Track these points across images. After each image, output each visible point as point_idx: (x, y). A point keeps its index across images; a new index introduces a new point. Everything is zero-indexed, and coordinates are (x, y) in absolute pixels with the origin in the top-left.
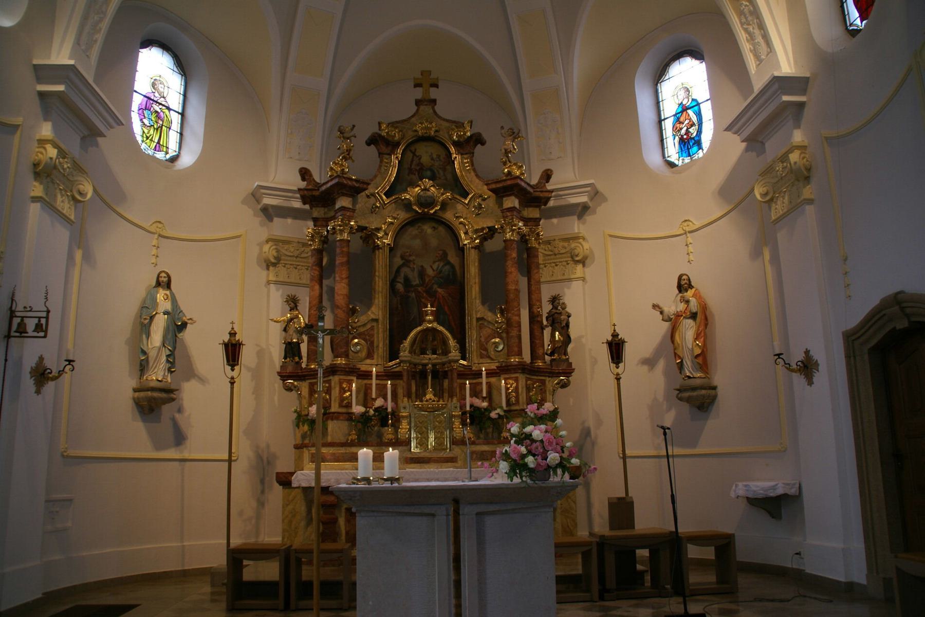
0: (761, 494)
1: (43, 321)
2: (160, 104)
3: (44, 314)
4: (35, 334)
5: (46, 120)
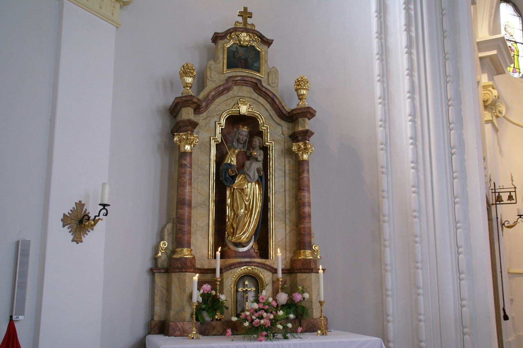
0: (179, 157)
1: (513, 194)
2: (511, 41)
3: (513, 190)
4: (509, 202)
5: (483, 73)
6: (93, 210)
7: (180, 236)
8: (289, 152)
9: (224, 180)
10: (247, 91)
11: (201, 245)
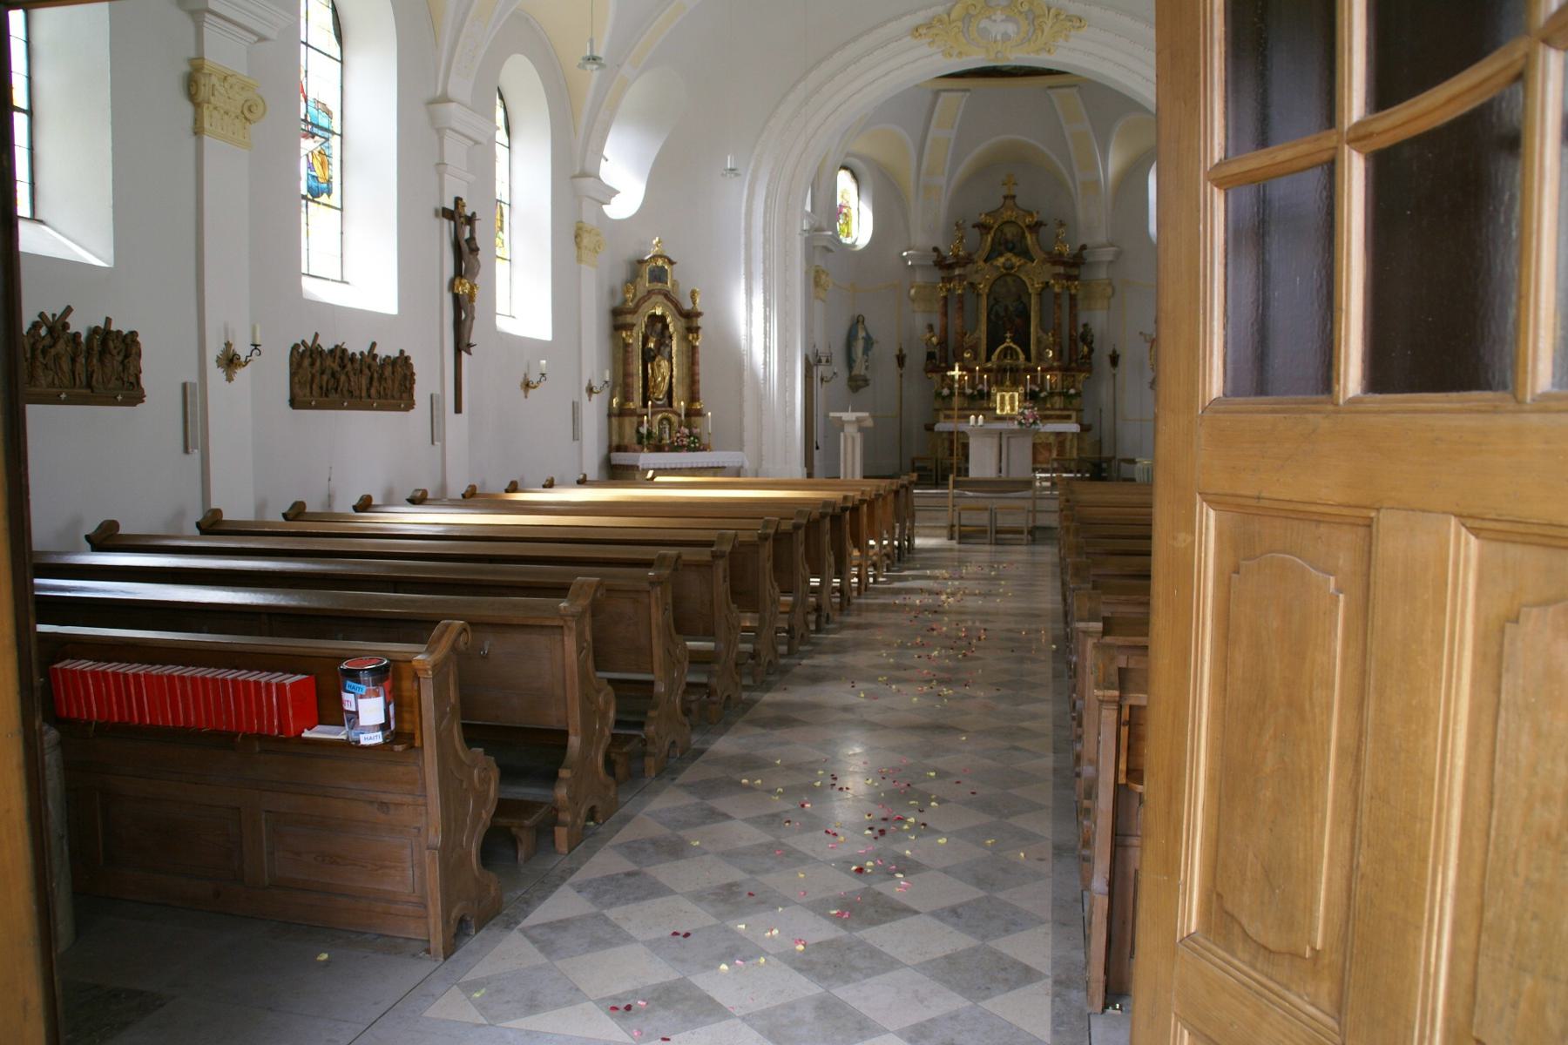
7: (626, 397)
8: (685, 338)
9: (648, 357)
10: (660, 298)
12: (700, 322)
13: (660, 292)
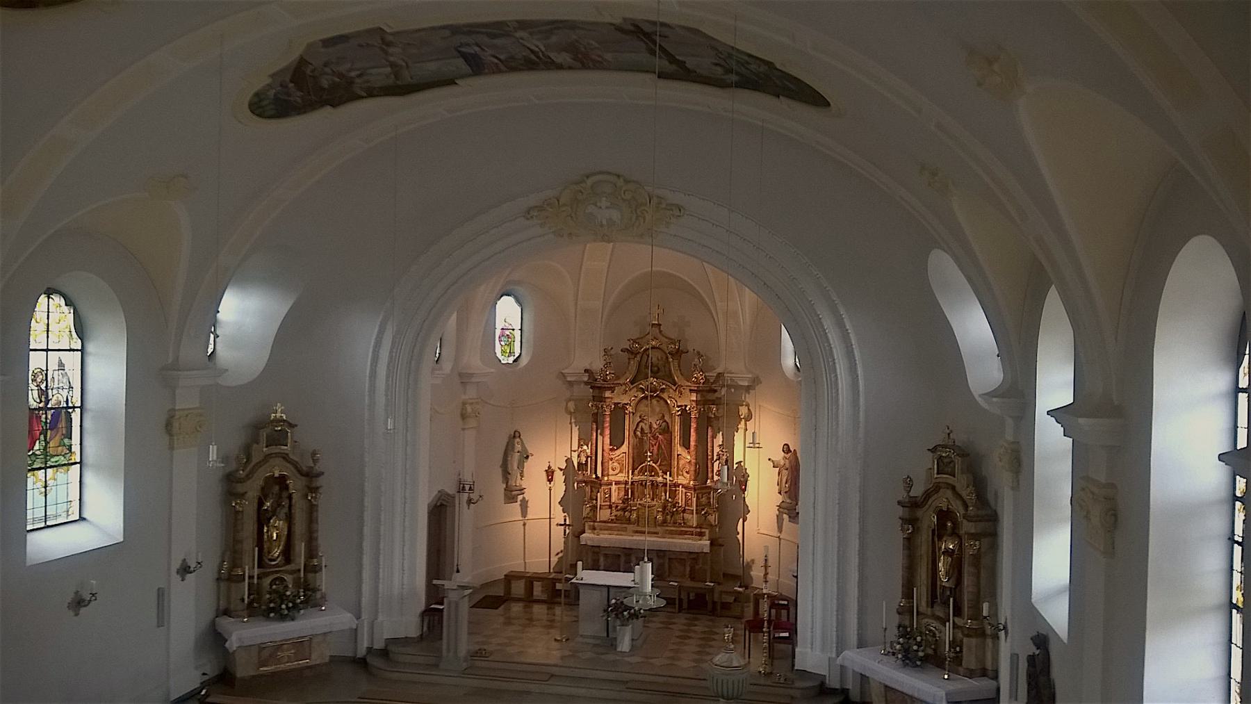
6: (193, 565)
7: (235, 564)
9: (263, 519)
10: (278, 461)
11: (249, 568)
12: (321, 481)
13: (277, 455)
